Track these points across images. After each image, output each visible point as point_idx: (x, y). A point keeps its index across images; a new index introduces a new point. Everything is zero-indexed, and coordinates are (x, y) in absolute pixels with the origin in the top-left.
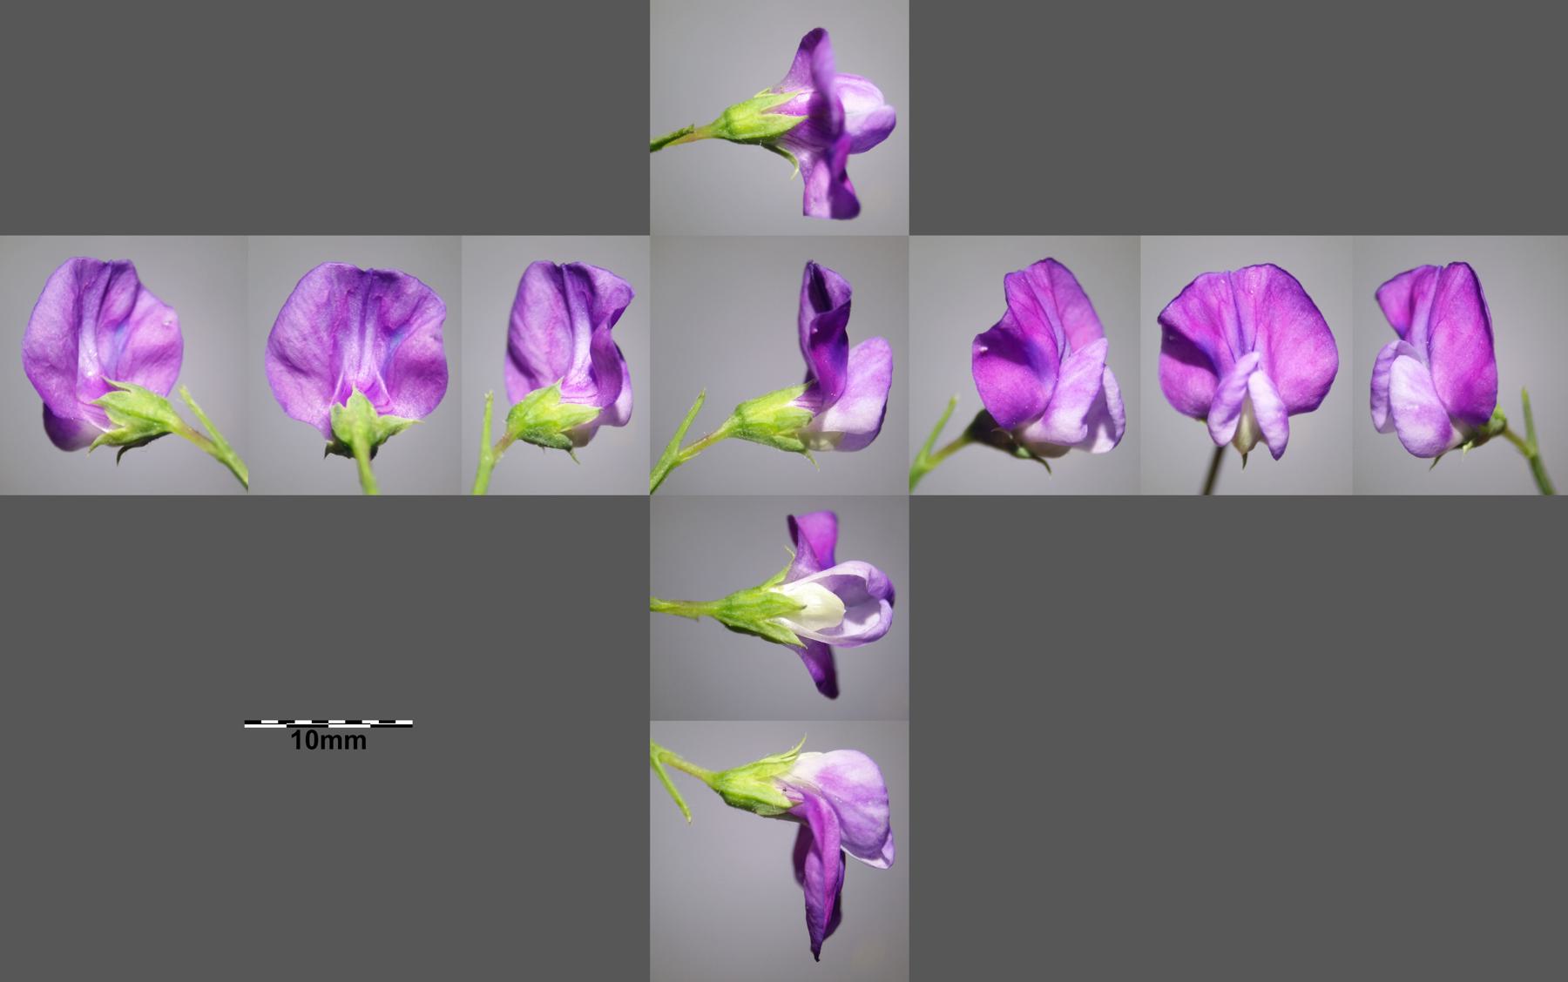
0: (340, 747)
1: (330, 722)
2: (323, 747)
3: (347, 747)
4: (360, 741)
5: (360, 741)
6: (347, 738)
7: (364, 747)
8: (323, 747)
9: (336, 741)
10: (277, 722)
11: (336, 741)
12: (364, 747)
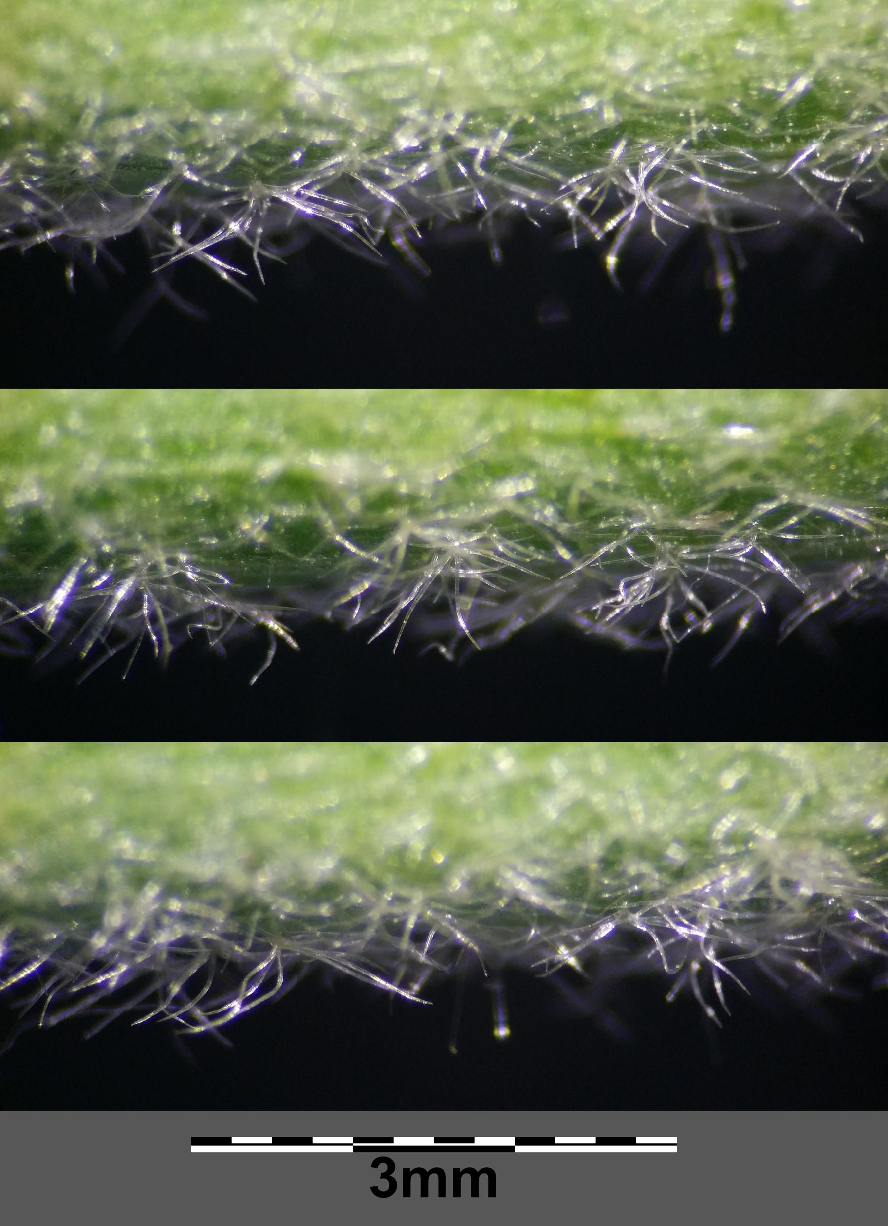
0: (442, 1193)
1: (350, 1149)
2: (407, 1193)
3: (457, 1193)
4: (484, 1179)
5: (484, 1179)
6: (457, 1174)
7: (492, 1193)
8: (407, 1193)
9: (434, 1179)
10: (593, 1140)
11: (434, 1179)
12: (492, 1193)
